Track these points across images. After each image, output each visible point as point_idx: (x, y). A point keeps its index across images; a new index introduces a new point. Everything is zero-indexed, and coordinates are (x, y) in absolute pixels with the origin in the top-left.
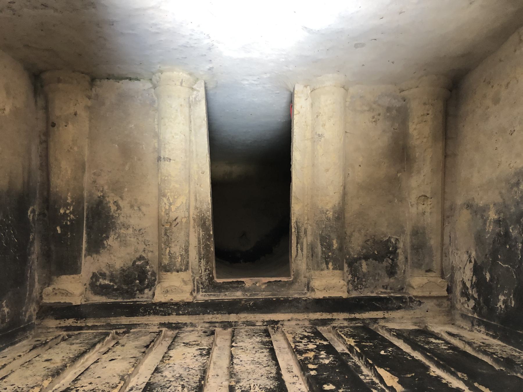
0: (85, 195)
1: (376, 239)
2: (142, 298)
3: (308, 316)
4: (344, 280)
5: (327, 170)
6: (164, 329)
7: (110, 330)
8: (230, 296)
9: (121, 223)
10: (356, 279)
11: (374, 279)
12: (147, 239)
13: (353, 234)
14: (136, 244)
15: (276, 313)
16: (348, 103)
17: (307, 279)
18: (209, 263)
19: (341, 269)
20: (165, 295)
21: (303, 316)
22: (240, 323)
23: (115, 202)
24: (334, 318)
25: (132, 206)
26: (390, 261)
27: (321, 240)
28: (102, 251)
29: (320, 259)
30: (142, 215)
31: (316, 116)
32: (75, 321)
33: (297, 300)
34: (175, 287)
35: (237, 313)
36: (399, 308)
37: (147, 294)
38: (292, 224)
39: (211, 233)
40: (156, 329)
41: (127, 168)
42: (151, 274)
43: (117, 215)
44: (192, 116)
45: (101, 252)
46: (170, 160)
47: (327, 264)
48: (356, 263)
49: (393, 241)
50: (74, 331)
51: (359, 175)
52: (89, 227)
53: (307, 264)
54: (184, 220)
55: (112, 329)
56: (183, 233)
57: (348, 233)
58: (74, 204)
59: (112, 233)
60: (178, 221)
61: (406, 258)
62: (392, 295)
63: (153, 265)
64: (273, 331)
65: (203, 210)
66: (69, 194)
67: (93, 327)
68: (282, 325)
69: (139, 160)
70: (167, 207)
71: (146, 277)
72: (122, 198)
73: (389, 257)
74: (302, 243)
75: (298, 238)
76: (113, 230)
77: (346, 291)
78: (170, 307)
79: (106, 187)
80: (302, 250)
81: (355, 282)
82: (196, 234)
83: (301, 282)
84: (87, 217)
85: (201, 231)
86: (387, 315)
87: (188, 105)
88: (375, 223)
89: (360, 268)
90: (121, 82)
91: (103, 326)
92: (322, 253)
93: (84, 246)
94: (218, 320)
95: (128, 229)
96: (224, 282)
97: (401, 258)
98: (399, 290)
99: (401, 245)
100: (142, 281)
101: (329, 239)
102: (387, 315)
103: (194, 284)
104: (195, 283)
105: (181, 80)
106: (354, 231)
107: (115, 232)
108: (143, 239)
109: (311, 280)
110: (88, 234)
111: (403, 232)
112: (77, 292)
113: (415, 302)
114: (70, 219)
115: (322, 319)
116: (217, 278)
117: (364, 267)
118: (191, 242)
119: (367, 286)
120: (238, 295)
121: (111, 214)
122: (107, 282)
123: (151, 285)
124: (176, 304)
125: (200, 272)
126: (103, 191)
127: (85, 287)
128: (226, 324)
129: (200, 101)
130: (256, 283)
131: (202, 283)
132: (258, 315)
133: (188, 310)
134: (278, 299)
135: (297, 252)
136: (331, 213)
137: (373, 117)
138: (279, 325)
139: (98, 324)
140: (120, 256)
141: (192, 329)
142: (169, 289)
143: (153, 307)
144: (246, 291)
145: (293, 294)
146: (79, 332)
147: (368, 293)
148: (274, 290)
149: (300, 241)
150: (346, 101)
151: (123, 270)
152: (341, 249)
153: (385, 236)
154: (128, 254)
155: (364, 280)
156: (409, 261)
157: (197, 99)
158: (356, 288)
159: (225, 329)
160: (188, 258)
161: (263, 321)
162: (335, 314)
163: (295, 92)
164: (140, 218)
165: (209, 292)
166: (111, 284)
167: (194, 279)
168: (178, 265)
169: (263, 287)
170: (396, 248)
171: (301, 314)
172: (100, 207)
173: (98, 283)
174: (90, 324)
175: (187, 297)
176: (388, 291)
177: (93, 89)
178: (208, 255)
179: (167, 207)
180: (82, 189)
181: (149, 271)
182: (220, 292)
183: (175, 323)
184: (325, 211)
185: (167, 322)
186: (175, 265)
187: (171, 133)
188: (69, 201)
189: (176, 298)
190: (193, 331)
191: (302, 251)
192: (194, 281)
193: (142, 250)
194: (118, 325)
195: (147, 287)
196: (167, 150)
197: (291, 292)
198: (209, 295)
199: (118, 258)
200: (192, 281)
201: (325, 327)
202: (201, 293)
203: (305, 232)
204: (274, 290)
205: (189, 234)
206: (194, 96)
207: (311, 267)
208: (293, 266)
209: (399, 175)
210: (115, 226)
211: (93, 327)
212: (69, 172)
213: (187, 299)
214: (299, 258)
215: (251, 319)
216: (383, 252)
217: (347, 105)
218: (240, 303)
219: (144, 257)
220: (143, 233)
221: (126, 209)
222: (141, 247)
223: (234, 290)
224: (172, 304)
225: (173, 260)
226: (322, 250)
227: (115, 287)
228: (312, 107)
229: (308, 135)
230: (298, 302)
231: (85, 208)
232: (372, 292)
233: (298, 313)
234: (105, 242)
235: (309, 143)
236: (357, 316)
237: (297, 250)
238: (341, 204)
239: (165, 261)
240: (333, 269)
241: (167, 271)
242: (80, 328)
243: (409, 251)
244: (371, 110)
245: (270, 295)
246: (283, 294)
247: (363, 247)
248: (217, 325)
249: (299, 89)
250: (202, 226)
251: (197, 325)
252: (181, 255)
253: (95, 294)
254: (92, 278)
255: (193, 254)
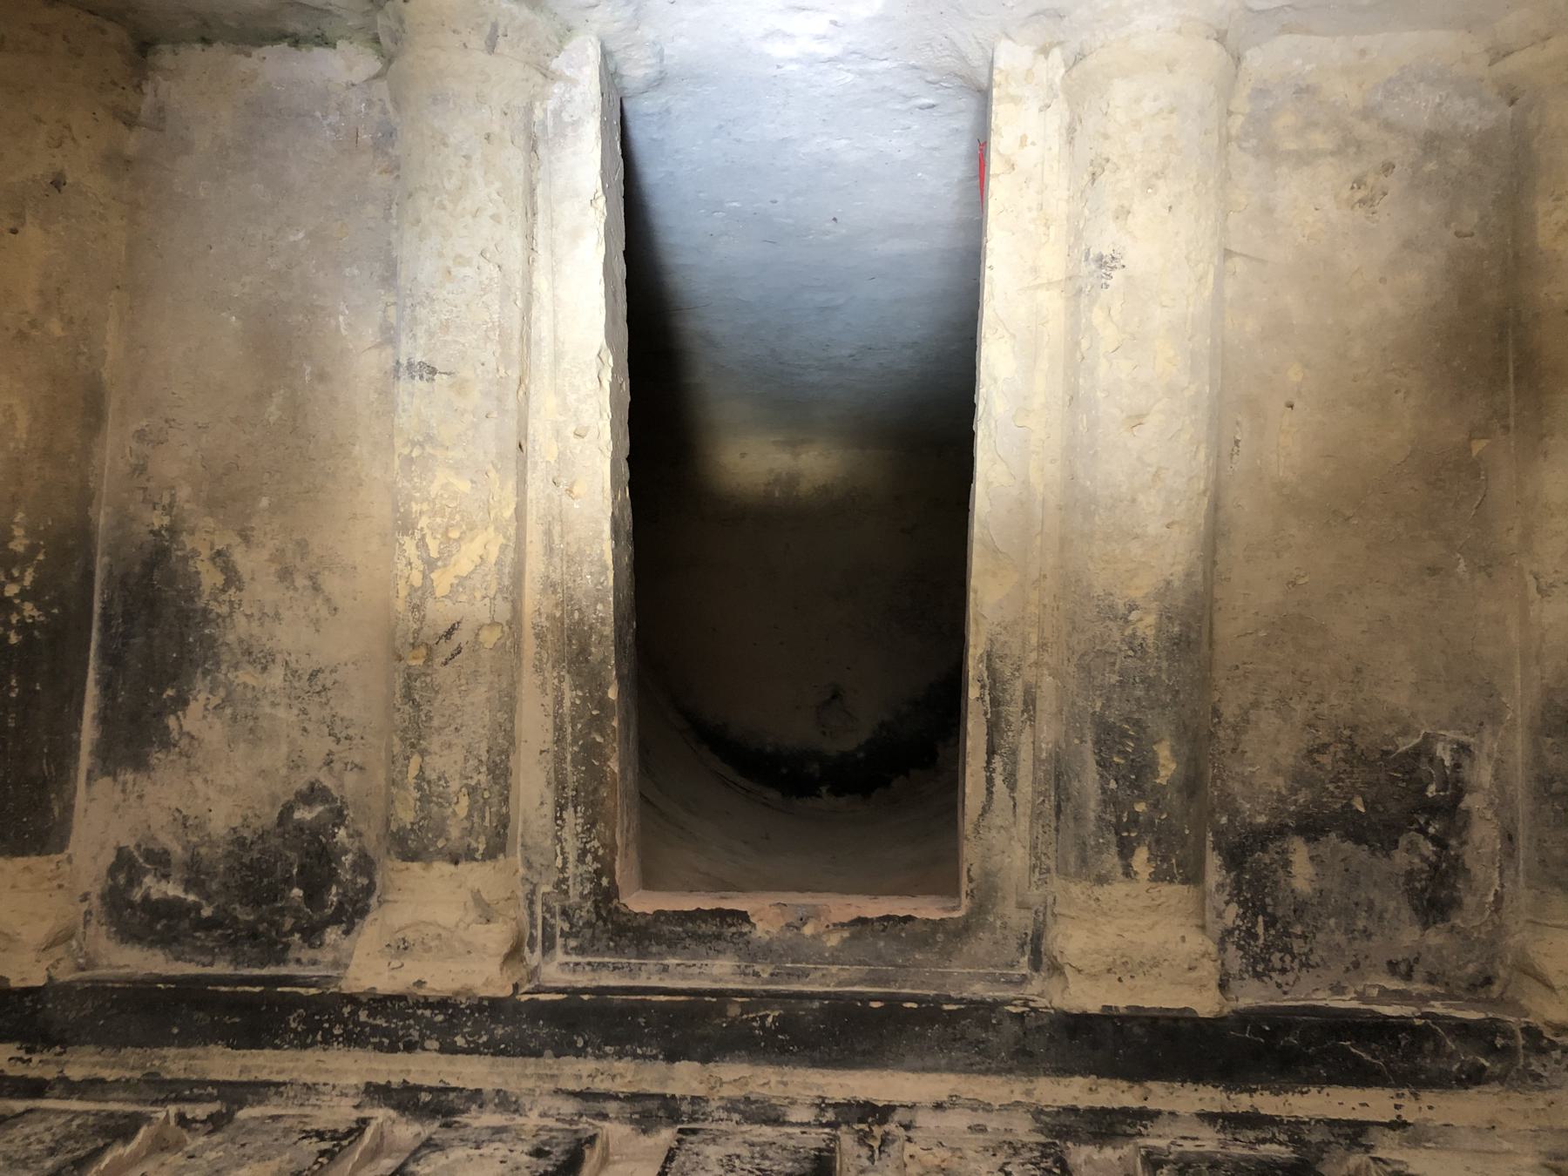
0: (102, 521)
1: (1361, 745)
2: (314, 963)
3: (1028, 1093)
4: (1203, 928)
5: (1137, 420)
6: (381, 1115)
7: (155, 1103)
8: (684, 977)
9: (241, 641)
10: (1265, 924)
11: (1349, 931)
12: (343, 713)
13: (1253, 715)
14: (296, 733)
15: (885, 1066)
16: (1237, 123)
17: (1030, 914)
18: (600, 826)
19: (1193, 876)
20: (395, 963)
21: (1004, 1091)
22: (714, 1105)
23: (219, 553)
24: (1151, 1105)
25: (285, 574)
26: (1428, 848)
27: (1097, 742)
28: (157, 757)
29: (1091, 827)
30: (324, 612)
31: (1087, 178)
32: (22, 1054)
33: (983, 1011)
34: (438, 931)
35: (705, 1059)
36: (1474, 1078)
37: (335, 947)
38: (971, 663)
39: (612, 694)
40: (338, 1113)
41: (273, 411)
42: (354, 865)
43: (225, 609)
44: (539, 190)
45: (154, 761)
46: (433, 371)
47: (1126, 850)
48: (1264, 849)
49: (1444, 753)
50: (11, 1096)
51: (1286, 447)
52: (111, 658)
53: (1034, 847)
54: (490, 638)
55: (163, 1102)
56: (480, 693)
57: (1229, 712)
58: (41, 557)
59: (201, 686)
60: (458, 638)
61: (1509, 838)
62: (1438, 1008)
63: (362, 827)
64: (865, 1152)
65: (579, 595)
66: (20, 516)
67: (90, 1087)
68: (907, 1127)
69: (322, 377)
70: (417, 579)
71: (332, 877)
72: (246, 538)
73: (1422, 831)
74: (1014, 752)
75: (994, 727)
76: (206, 673)
77: (1213, 984)
78: (413, 1016)
79: (184, 492)
80: (1011, 781)
81: (1255, 937)
82: (549, 700)
83: (1005, 926)
84: (106, 619)
85: (566, 686)
86: (1412, 1111)
87: (521, 140)
88: (1359, 671)
89: (1281, 872)
90: (257, 53)
91: (126, 1084)
92: (1104, 803)
93: (88, 733)
94: (618, 1086)
95: (264, 669)
96: (659, 913)
97: (1484, 835)
98: (1473, 987)
99: (1482, 774)
100: (314, 895)
101: (1137, 740)
102: (1412, 1111)
103: (532, 914)
104: (538, 909)
105: (488, 29)
106: (1256, 705)
107: (214, 679)
108: (327, 712)
109: (1049, 919)
110: (107, 686)
111: (1494, 716)
112: (37, 932)
113: (1557, 1054)
114: (22, 621)
115: (1091, 1110)
116: (649, 881)
117: (1302, 869)
118: (537, 733)
119: (1314, 959)
120: (719, 971)
121: (201, 604)
122: (173, 890)
123: (352, 913)
124: (443, 1004)
125: (559, 863)
126: (171, 505)
127: (84, 907)
128: (652, 1105)
129: (576, 124)
130: (803, 921)
131: (564, 913)
132: (800, 1071)
133: (491, 1033)
134: (893, 1001)
135: (990, 792)
136: (1151, 619)
137: (1359, 183)
138: (890, 1127)
139: (110, 1075)
140: (230, 782)
141: (498, 1120)
142: (411, 936)
143: (346, 1010)
144: (753, 958)
145: (967, 979)
146: (29, 1104)
147: (1314, 992)
148: (879, 957)
149: (1004, 743)
150: (1230, 113)
151: (241, 842)
152: (1191, 785)
153: (1405, 732)
154: (262, 773)
155: (1298, 929)
156: (1522, 854)
157: (566, 117)
158: (1259, 967)
159: (645, 1132)
160: (506, 800)
161: (821, 1105)
162: (1155, 1086)
163: (997, 77)
164: (316, 623)
165: (597, 953)
166: (191, 898)
167: (533, 892)
168: (455, 833)
169: (833, 940)
170: (1457, 788)
171: (996, 1080)
172: (157, 575)
173: (137, 895)
174: (75, 1073)
175: (484, 975)
176: (1418, 987)
177: (148, 88)
178: (596, 790)
179: (417, 579)
180: (85, 498)
181: (346, 852)
182: (643, 954)
183: (430, 1090)
184: (1122, 610)
185: (396, 1081)
186: (441, 831)
187: (441, 255)
188: (18, 545)
189: (441, 977)
190: (498, 1131)
191: (1012, 787)
192: (531, 903)
193: (319, 760)
194: (192, 1084)
195: (335, 920)
196: (420, 331)
197: (956, 969)
198: (595, 967)
199: (222, 790)
200: (523, 903)
201: (1109, 1152)
202: (560, 956)
203: (1030, 702)
204: (879, 957)
205: (512, 698)
206: (551, 105)
207: (1052, 864)
208: (970, 854)
209: (1478, 446)
210: (216, 655)
211: (90, 1087)
212: (23, 422)
213: (487, 984)
214: (998, 817)
215: (765, 1091)
216: (1397, 806)
217: (1233, 132)
218: (722, 1013)
219: (325, 789)
220: (325, 688)
221: (262, 588)
222: (317, 746)
223: (702, 950)
224: (427, 1004)
225: (435, 809)
226: (1104, 791)
227: (207, 912)
228: (1071, 141)
229: (1053, 263)
230: (985, 1024)
231: (99, 576)
232: (1338, 989)
233: (986, 1072)
234: (172, 722)
235: (1053, 303)
236: (1266, 1103)
237: (990, 781)
238: (1199, 578)
239: (402, 814)
240: (1156, 877)
241: (411, 856)
242: (37, 1088)
243: (1523, 806)
244: (1349, 146)
245: (861, 982)
246: (916, 982)
247: (1299, 780)
248: (612, 1107)
249: (1012, 57)
250: (571, 663)
251: (526, 1101)
252: (472, 791)
253: (123, 941)
254: (113, 871)
255: (532, 788)
